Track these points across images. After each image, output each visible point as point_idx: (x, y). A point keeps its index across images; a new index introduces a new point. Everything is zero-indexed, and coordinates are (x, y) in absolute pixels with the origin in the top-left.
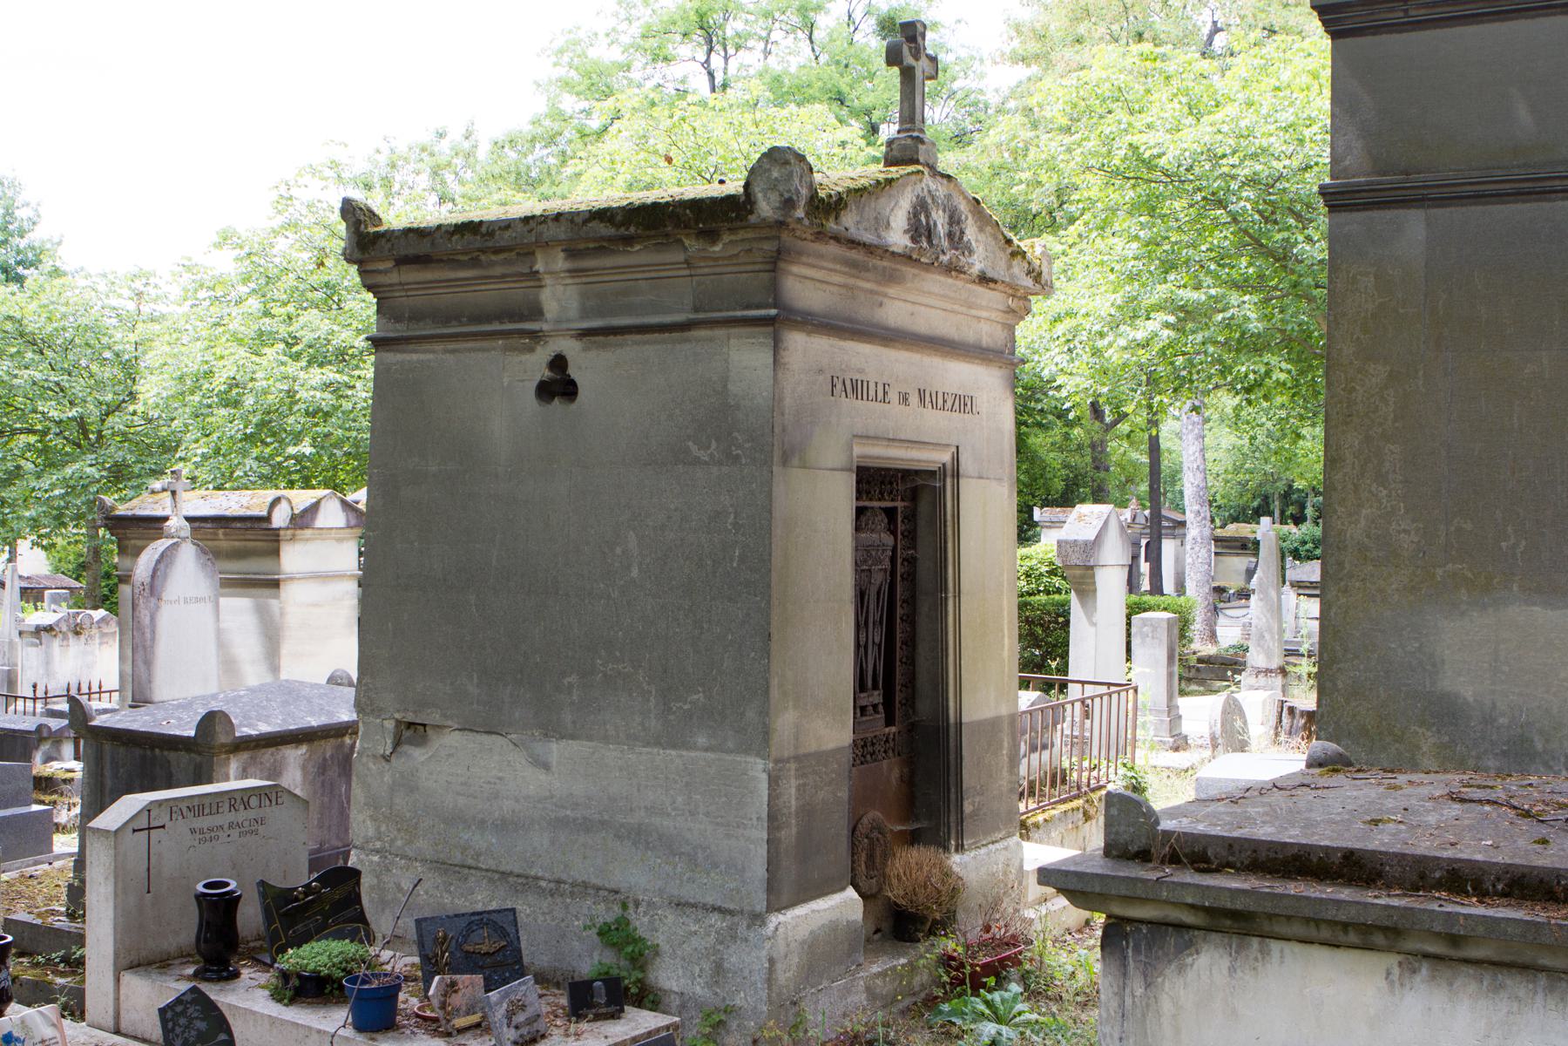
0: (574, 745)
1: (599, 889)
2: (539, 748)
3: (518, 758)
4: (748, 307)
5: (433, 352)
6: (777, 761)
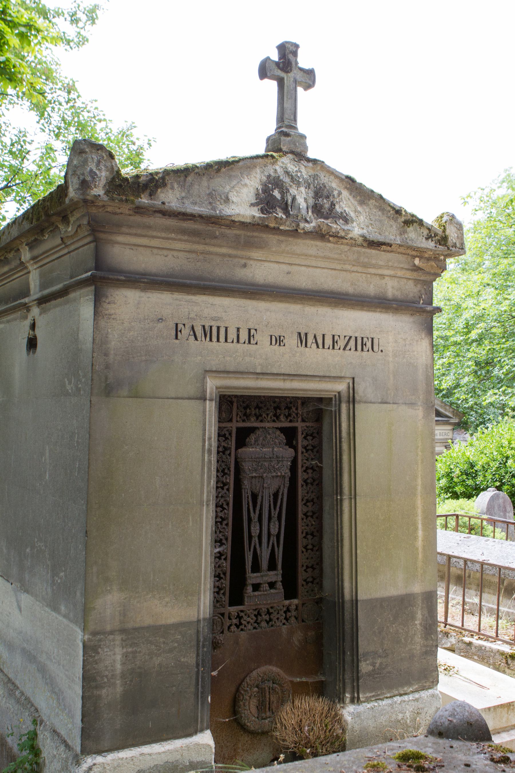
6: (94, 634)
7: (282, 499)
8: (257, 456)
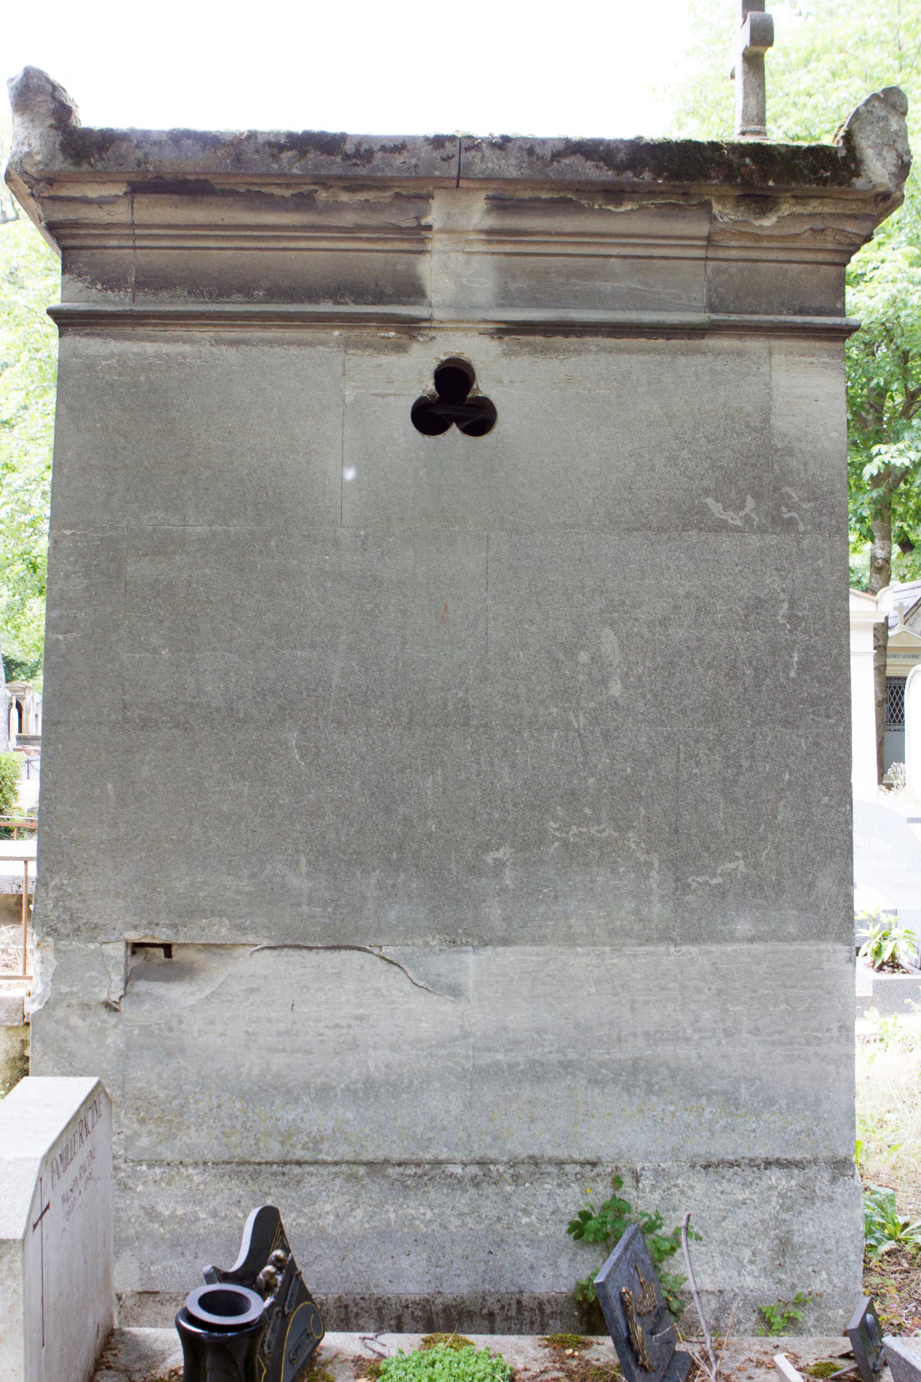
0: (510, 955)
1: (560, 1164)
2: (443, 964)
3: (394, 984)
4: (801, 312)
5: (192, 341)
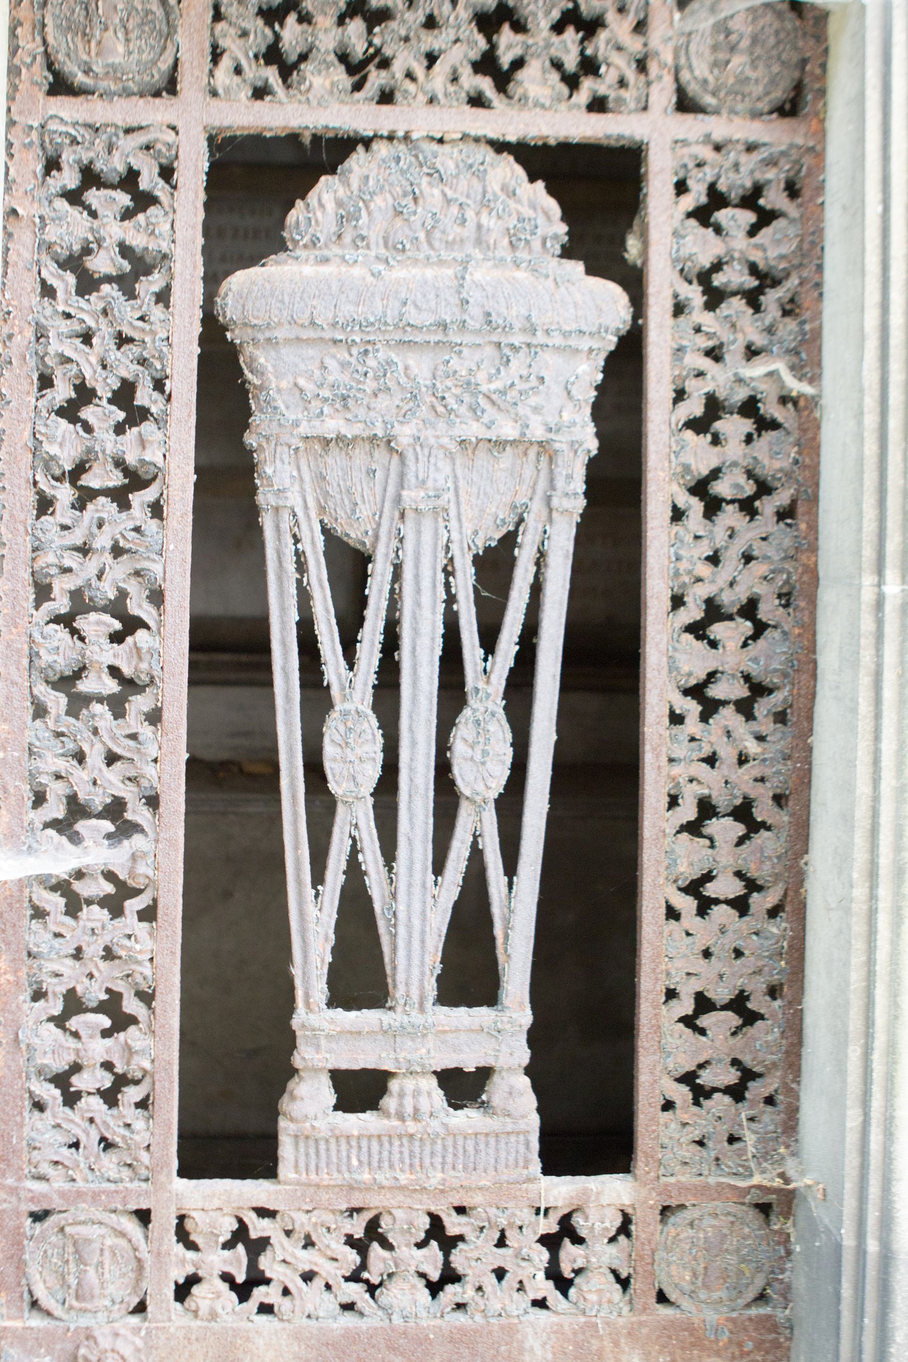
7: (537, 589)
8: (347, 311)
